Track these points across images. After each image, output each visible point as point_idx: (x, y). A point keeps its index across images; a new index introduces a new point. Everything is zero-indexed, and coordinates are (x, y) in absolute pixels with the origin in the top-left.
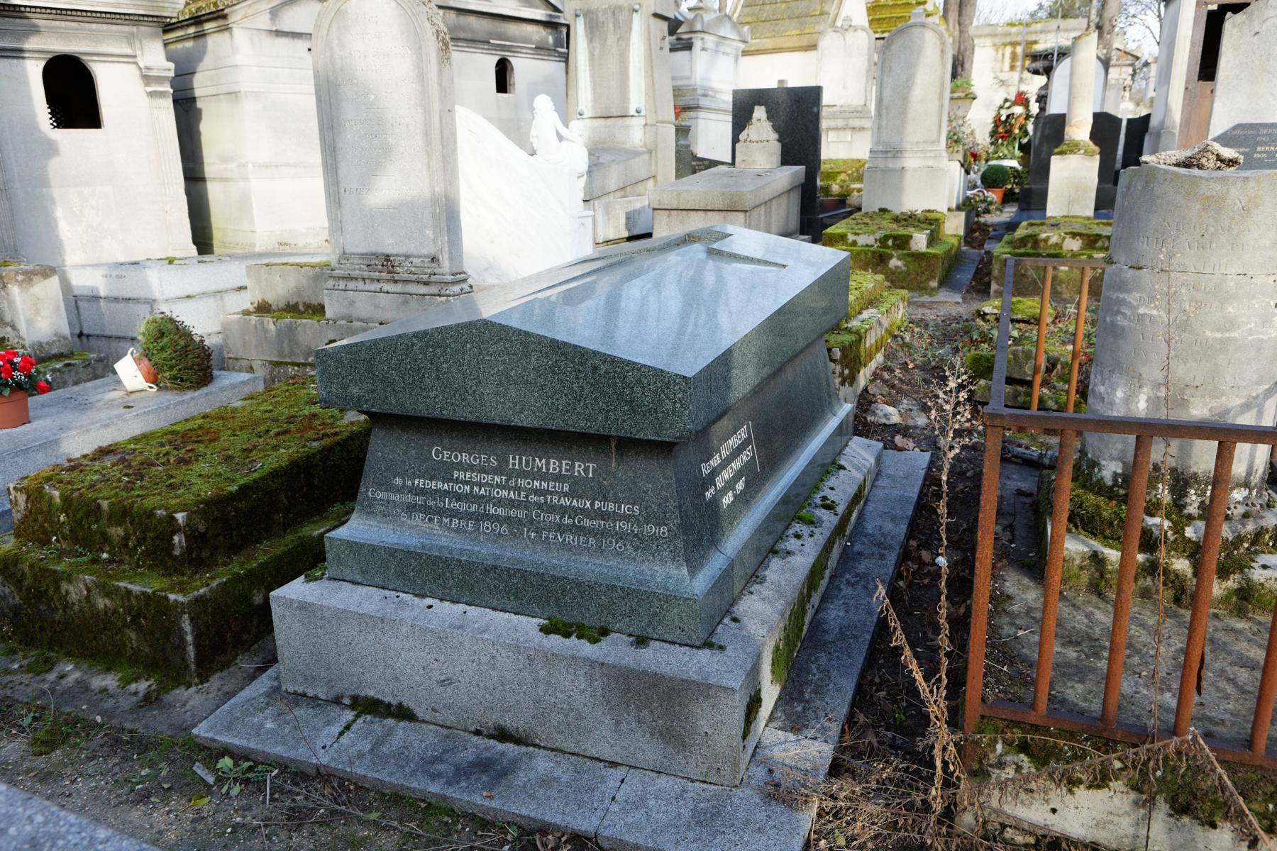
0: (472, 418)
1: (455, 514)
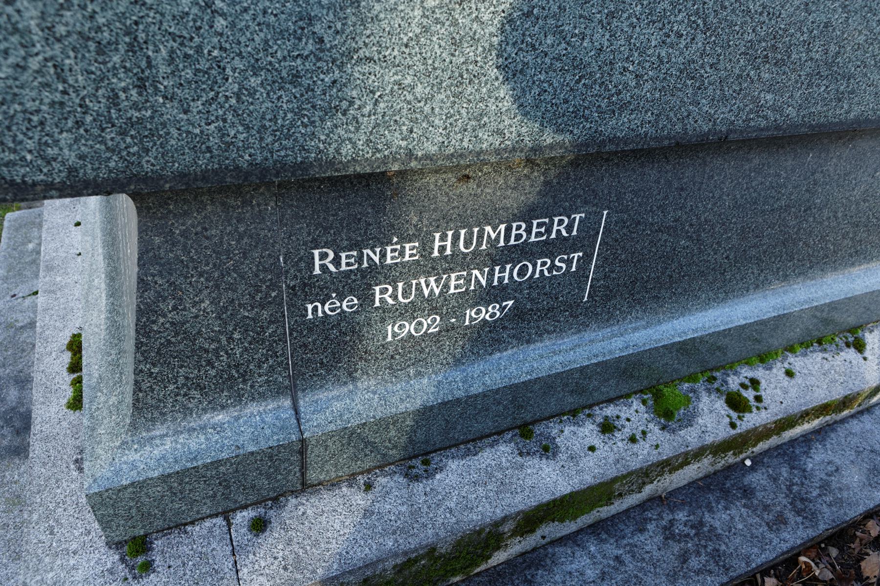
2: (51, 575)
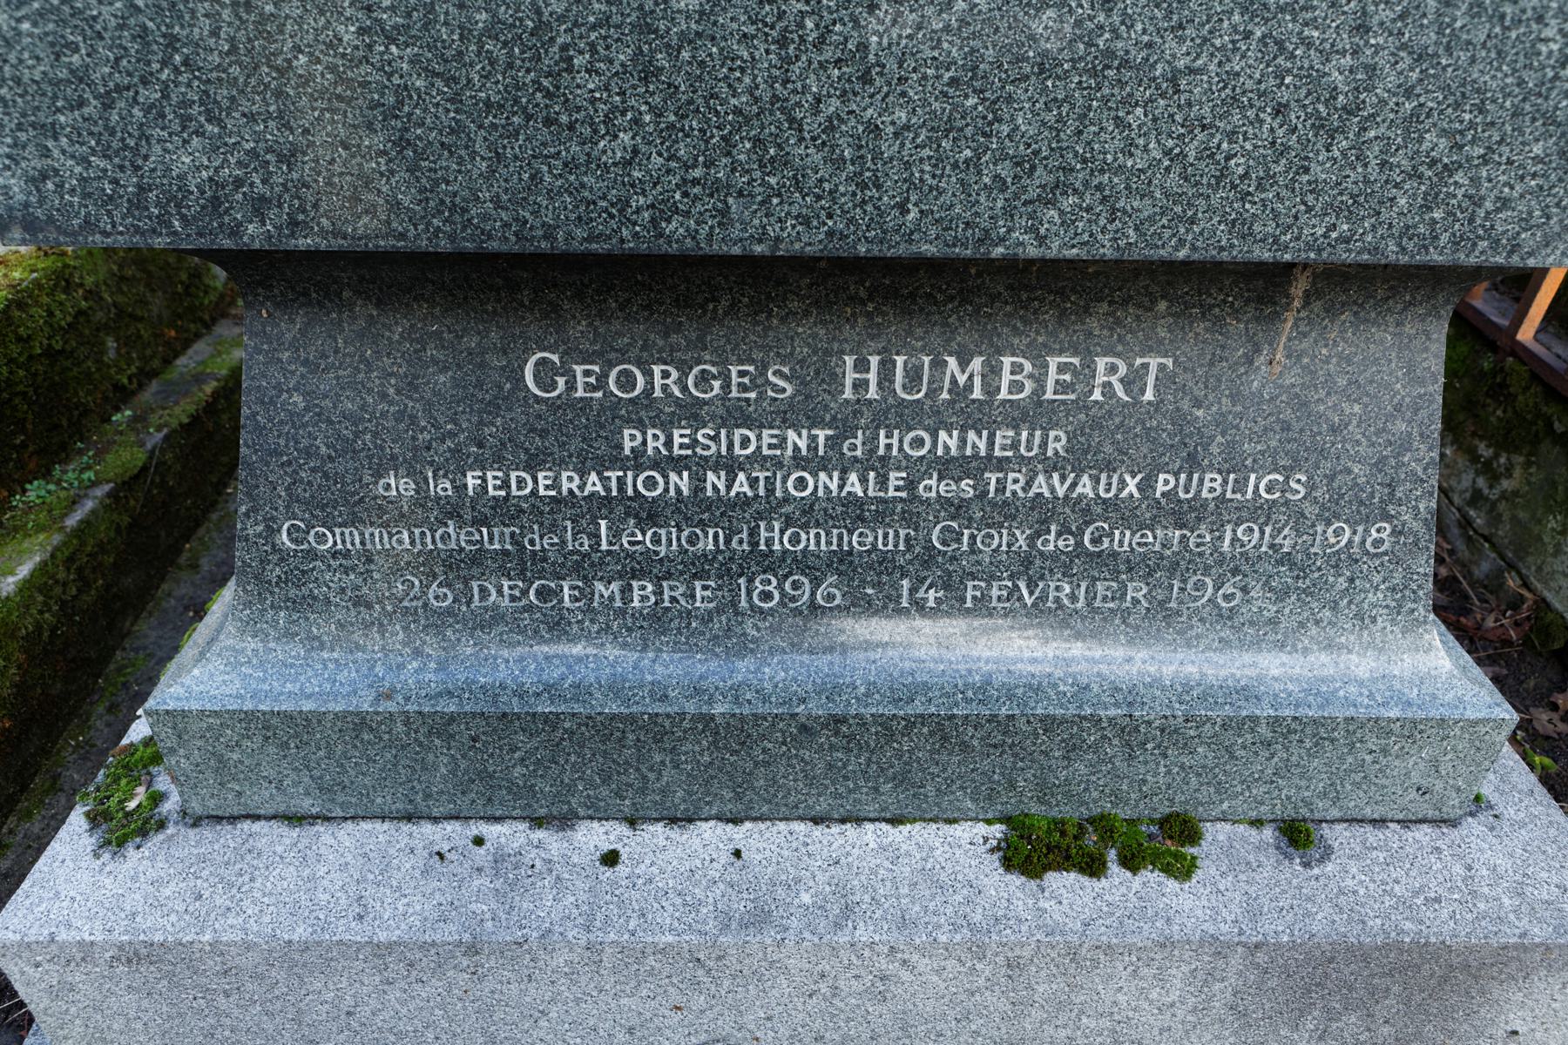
0: (811, 242)
1: (637, 567)
2: (1506, 901)
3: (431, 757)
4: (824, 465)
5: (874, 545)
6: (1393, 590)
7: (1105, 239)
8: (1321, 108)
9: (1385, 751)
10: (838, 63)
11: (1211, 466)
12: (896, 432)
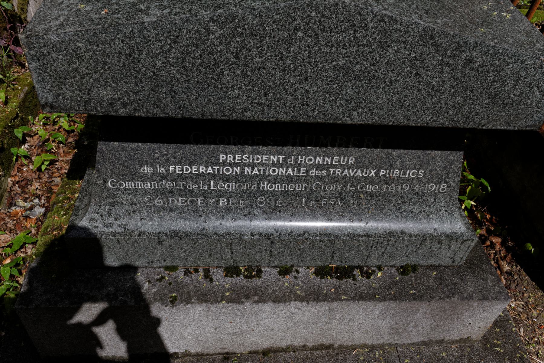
1: (221, 194)
3: (156, 251)
4: (281, 166)
5: (295, 189)
6: (446, 202)
7: (370, 120)
8: (430, 90)
9: (440, 248)
10: (299, 76)
11: (396, 168)
12: (304, 157)
